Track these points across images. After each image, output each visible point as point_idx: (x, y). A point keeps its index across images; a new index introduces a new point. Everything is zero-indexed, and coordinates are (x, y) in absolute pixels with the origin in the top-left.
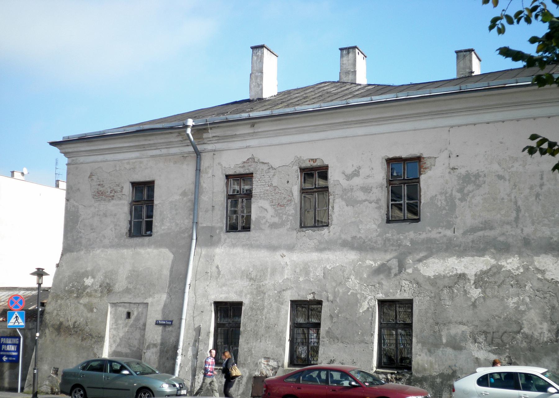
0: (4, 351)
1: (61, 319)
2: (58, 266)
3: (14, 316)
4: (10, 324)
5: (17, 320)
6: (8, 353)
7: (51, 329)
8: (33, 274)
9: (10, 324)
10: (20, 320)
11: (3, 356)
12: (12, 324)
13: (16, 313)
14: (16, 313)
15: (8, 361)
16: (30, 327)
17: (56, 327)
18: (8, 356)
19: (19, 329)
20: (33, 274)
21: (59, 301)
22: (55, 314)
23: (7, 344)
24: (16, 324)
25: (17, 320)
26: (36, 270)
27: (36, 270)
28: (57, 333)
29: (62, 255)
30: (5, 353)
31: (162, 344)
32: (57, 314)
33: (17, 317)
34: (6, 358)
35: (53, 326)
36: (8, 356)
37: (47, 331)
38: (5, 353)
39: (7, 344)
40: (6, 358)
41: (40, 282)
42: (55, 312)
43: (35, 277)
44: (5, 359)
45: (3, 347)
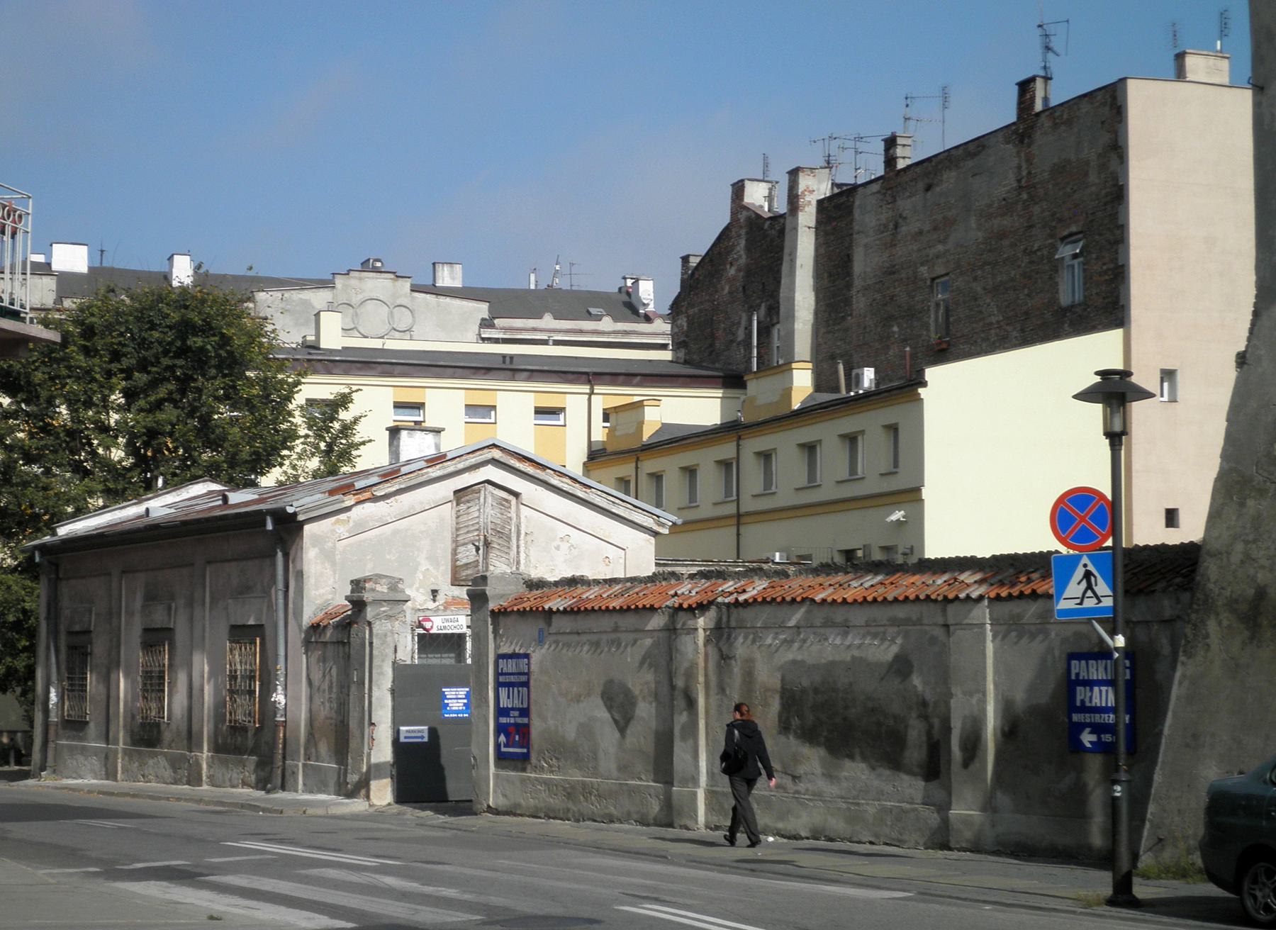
0: (1084, 709)
1: (1262, 577)
2: (1242, 359)
3: (1080, 572)
4: (1063, 605)
5: (1089, 587)
6: (1098, 718)
7: (1226, 618)
8: (1086, 396)
9: (1063, 605)
10: (1102, 588)
11: (1081, 727)
12: (1071, 605)
13: (1085, 560)
14: (1085, 560)
15: (1099, 747)
16: (1168, 613)
17: (1244, 607)
18: (1098, 729)
19: (1100, 621)
20: (1086, 396)
21: (1250, 503)
22: (1236, 557)
23: (1090, 684)
24: (1090, 603)
25: (1089, 587)
26: (1098, 379)
27: (1098, 379)
28: (1247, 633)
29: (1256, 314)
30: (1087, 718)
31: (783, 688)
32: (1248, 558)
33: (1088, 575)
34: (1093, 738)
35: (1232, 604)
36: (1098, 729)
37: (1212, 625)
38: (1087, 718)
39: (1090, 684)
40: (1093, 738)
41: (1117, 427)
42: (1240, 547)
43: (1097, 409)
44: (1087, 738)
45: (1081, 693)
